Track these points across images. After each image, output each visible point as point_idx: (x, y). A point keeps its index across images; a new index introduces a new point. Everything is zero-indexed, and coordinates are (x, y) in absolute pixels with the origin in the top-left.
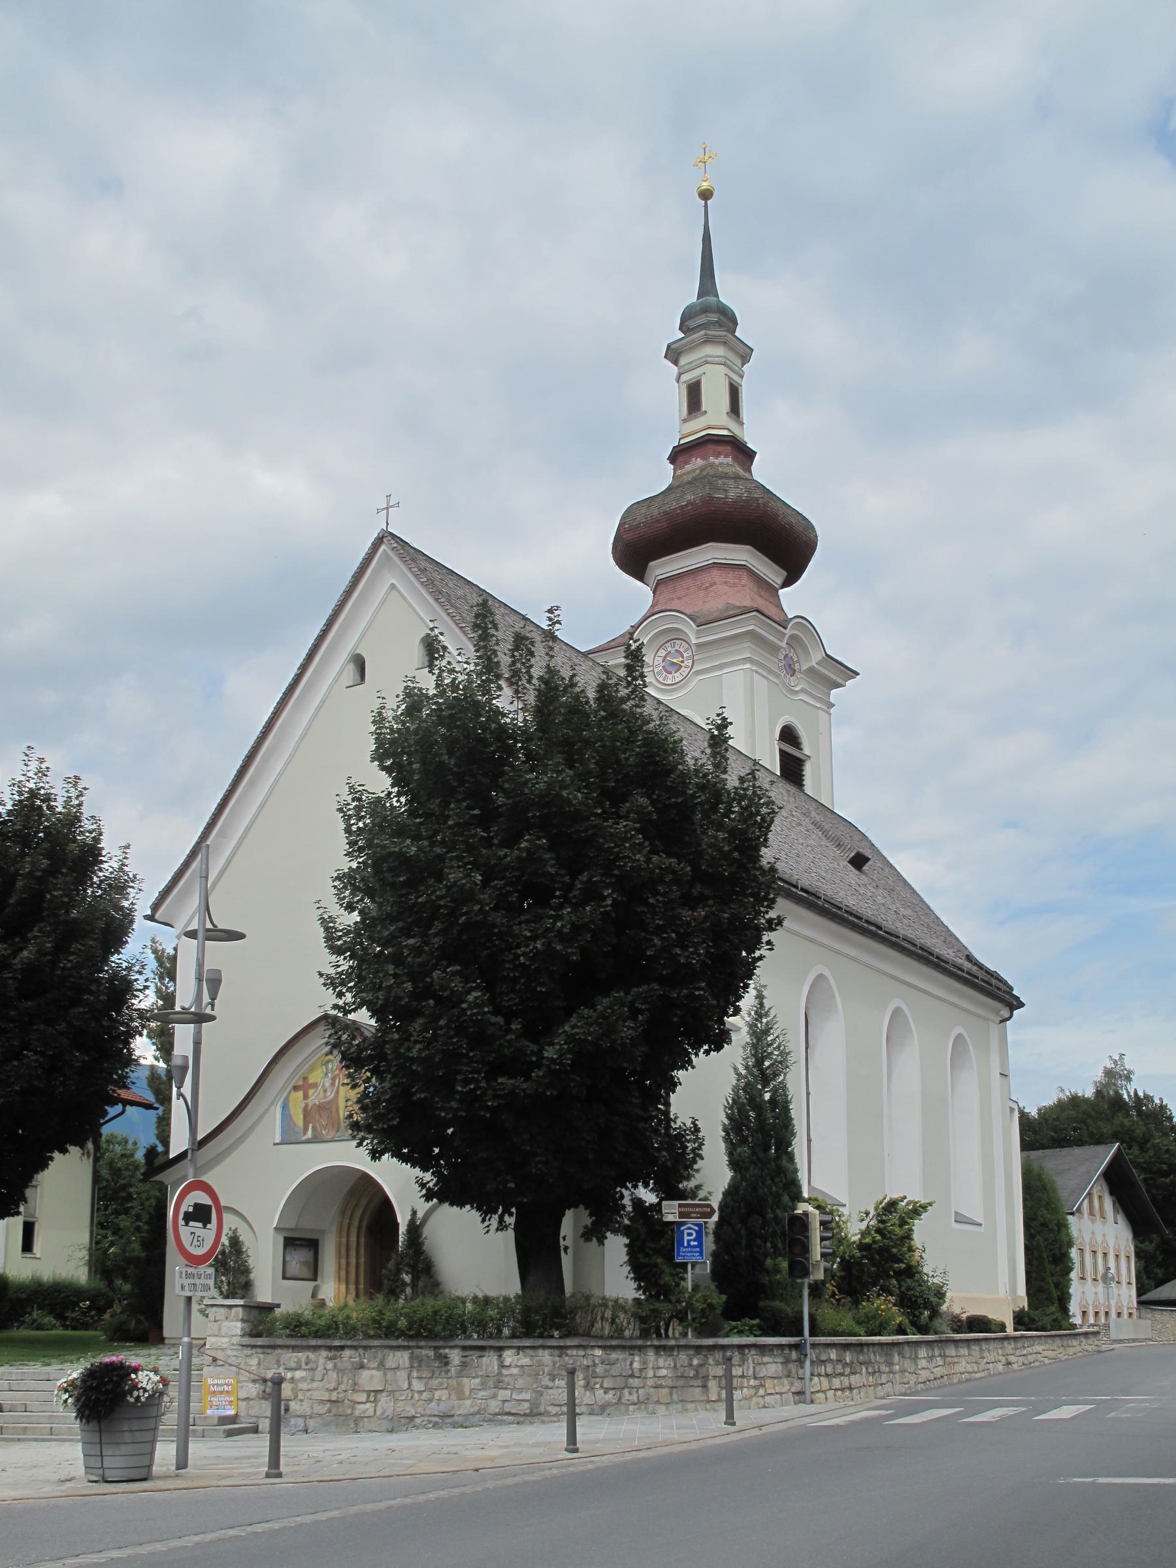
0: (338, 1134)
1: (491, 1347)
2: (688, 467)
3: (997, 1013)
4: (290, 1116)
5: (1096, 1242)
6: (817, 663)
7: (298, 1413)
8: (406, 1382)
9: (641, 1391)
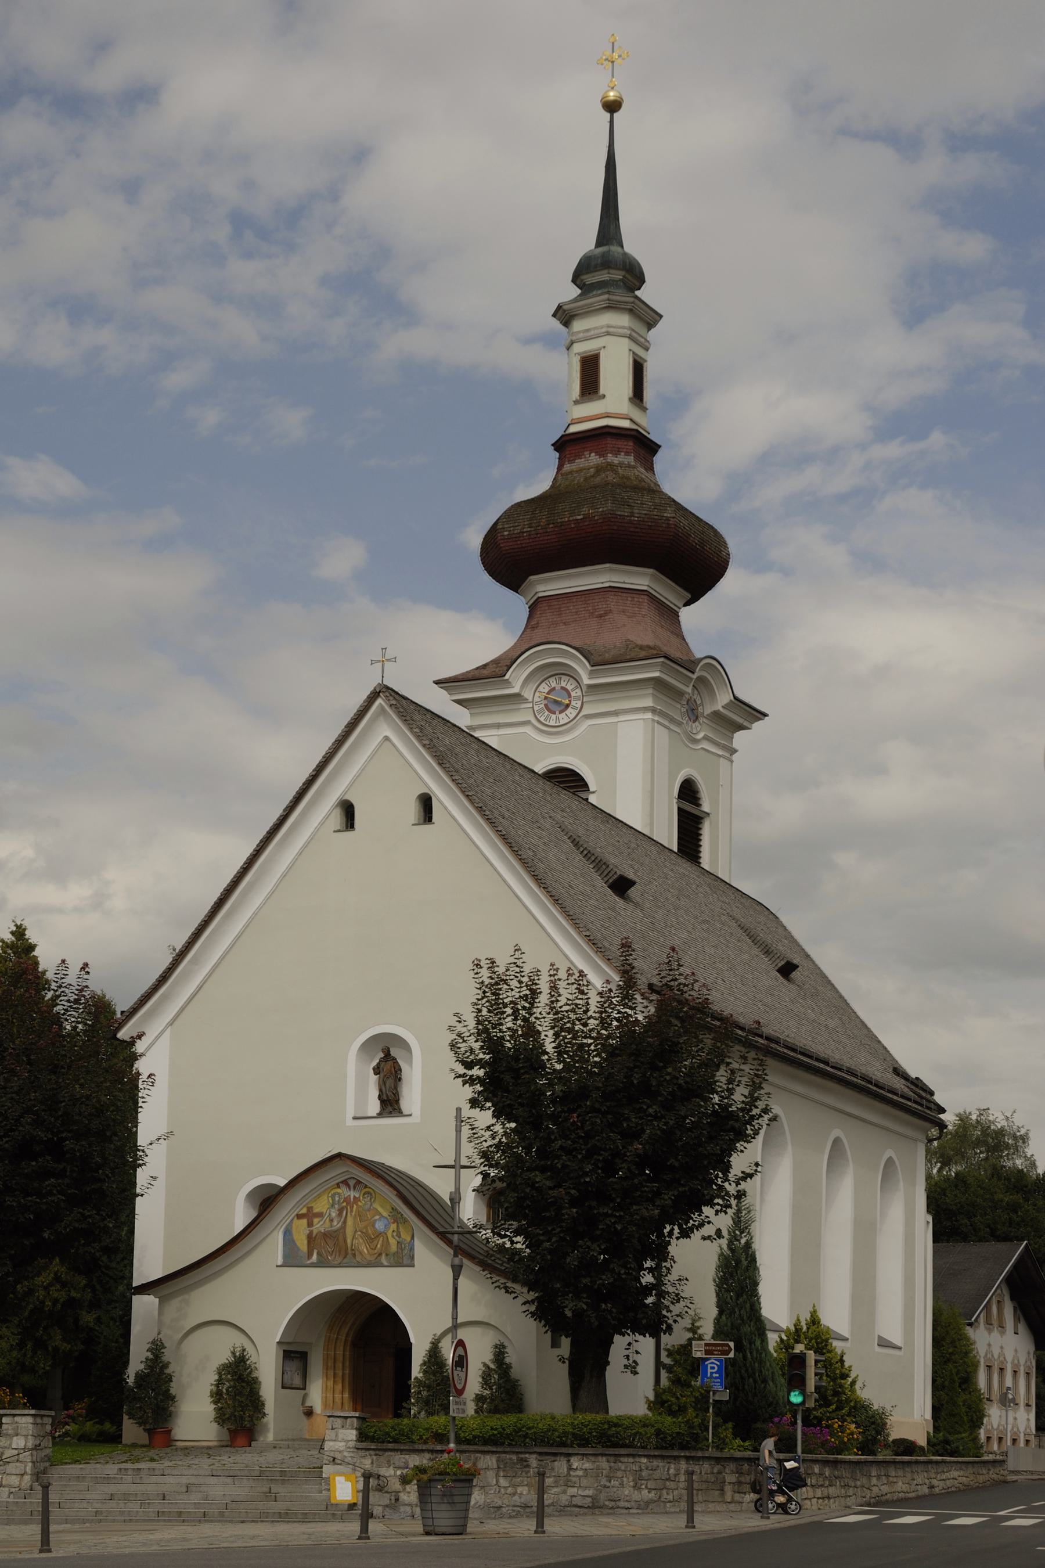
0: (345, 1260)
1: (561, 1454)
2: (580, 463)
3: (926, 1131)
4: (294, 1241)
5: (992, 1356)
6: (723, 707)
7: (407, 1502)
8: (495, 1480)
9: (676, 1492)
